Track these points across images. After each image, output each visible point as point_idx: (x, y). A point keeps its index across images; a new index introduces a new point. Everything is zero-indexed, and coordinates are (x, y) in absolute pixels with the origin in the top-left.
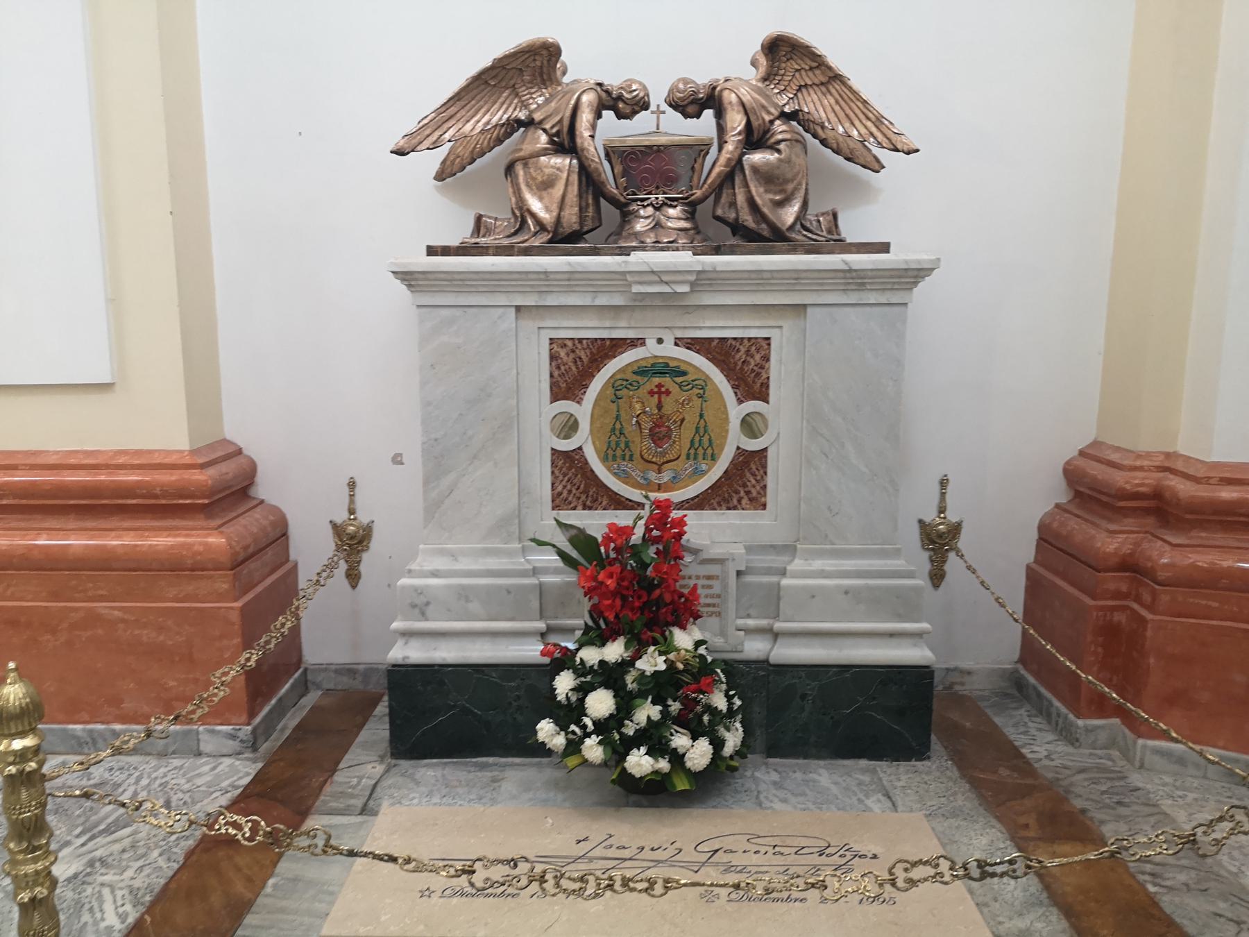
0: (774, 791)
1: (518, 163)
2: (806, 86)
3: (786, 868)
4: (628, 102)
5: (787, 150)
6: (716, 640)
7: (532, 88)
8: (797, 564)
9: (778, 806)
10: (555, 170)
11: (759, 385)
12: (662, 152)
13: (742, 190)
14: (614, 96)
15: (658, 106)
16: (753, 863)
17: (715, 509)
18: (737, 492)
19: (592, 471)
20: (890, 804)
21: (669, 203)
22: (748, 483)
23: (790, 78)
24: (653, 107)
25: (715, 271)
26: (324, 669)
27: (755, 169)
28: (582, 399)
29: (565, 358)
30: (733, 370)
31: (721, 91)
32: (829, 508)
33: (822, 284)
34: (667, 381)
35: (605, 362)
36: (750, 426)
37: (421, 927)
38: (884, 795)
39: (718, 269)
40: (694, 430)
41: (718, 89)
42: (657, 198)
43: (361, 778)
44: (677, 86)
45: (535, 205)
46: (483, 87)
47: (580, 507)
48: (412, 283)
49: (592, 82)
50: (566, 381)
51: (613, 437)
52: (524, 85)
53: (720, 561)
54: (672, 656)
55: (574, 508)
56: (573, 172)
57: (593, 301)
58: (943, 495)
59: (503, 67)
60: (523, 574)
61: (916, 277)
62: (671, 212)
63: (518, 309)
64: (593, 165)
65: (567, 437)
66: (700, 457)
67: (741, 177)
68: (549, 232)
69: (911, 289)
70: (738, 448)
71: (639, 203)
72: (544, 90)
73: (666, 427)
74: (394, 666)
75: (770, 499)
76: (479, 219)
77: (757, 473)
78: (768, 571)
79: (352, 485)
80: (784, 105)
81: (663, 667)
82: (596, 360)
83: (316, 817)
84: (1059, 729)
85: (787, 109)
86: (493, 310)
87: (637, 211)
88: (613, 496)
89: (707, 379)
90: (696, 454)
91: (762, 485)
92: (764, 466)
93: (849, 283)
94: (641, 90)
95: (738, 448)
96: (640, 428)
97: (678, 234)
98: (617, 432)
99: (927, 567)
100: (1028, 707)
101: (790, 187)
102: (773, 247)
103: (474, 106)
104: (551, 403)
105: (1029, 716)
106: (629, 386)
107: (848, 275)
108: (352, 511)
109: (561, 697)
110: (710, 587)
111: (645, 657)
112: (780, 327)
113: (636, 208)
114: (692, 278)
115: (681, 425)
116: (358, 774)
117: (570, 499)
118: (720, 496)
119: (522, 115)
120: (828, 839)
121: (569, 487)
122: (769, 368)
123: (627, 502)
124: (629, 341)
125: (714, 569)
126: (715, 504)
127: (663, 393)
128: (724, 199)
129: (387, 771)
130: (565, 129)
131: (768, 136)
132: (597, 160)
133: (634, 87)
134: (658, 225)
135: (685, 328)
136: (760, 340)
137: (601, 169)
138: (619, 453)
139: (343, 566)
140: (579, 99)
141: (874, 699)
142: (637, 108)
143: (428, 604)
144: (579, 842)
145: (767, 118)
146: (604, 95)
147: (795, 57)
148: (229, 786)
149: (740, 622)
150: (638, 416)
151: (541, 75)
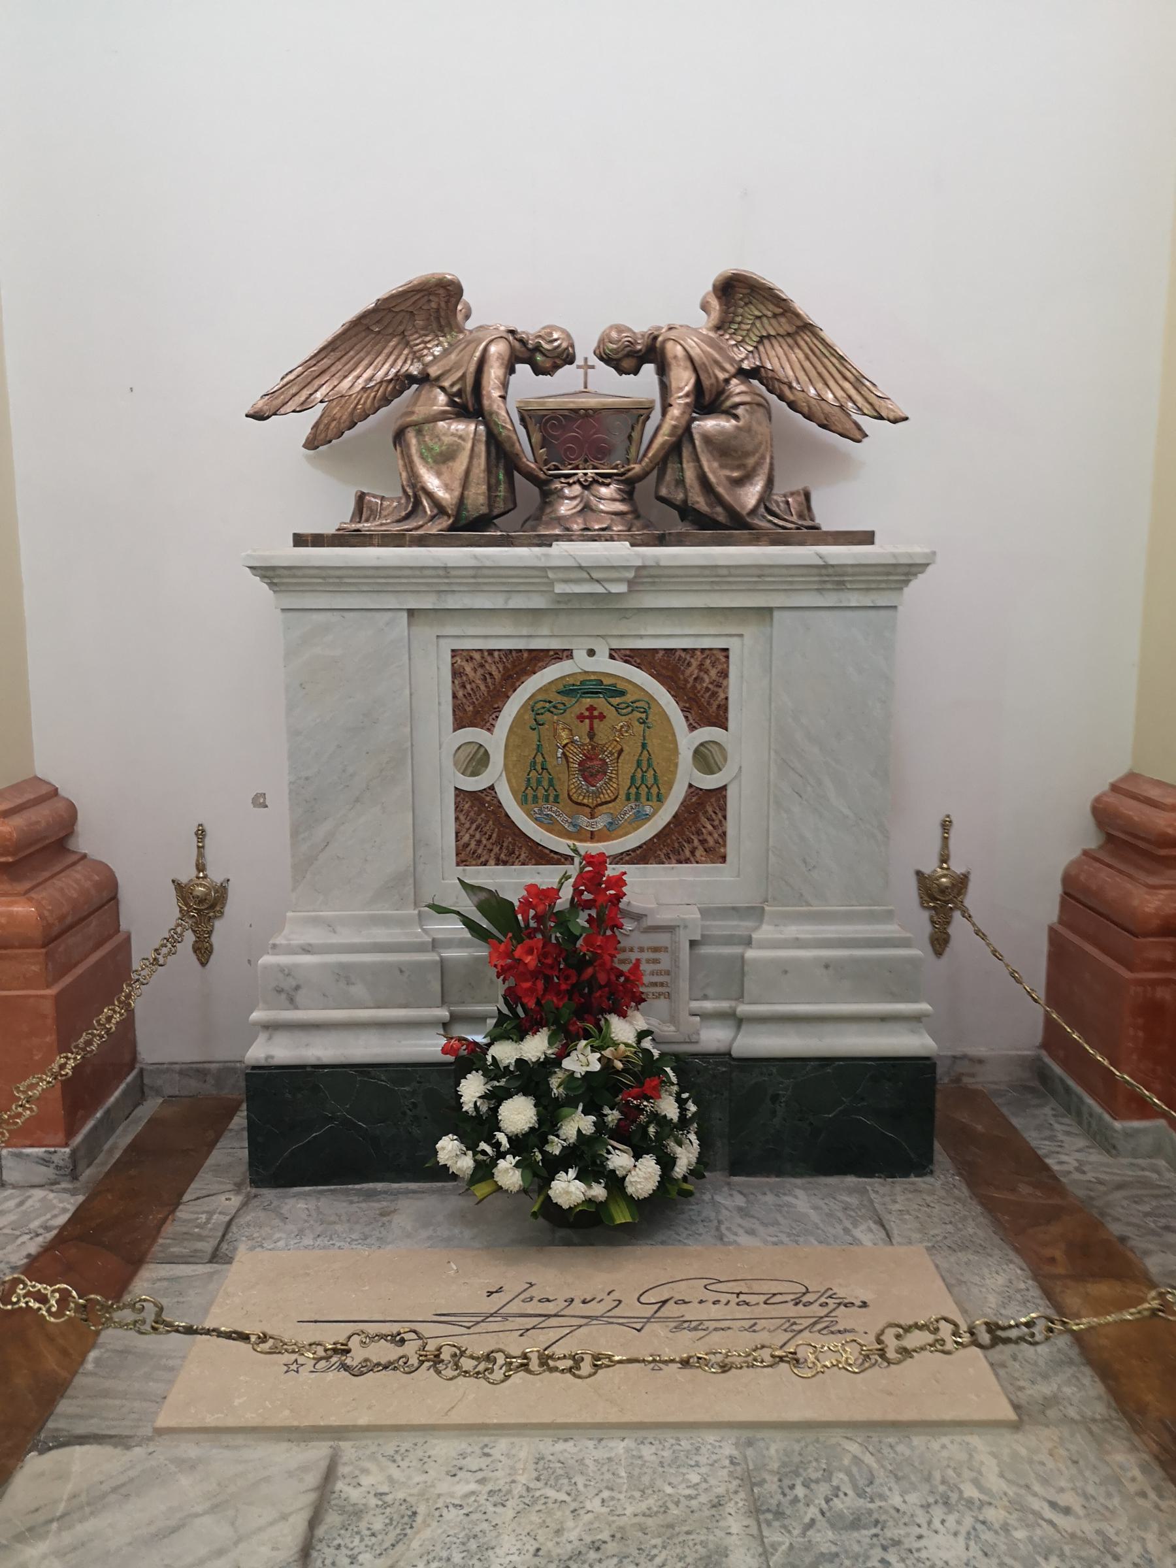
0: (740, 1221)
1: (409, 429)
2: (769, 337)
3: (753, 1322)
4: (546, 352)
5: (747, 416)
6: (666, 1029)
7: (426, 335)
8: (766, 932)
9: (744, 1239)
10: (456, 439)
11: (715, 707)
12: (591, 416)
13: (691, 464)
14: (530, 346)
15: (586, 359)
17: (663, 863)
18: (689, 841)
19: (507, 815)
20: (883, 1234)
21: (601, 480)
23: (749, 327)
24: (579, 361)
25: (659, 567)
27: (707, 439)
28: (493, 725)
29: (471, 674)
31: (664, 341)
32: (805, 861)
33: (791, 583)
34: (600, 702)
35: (523, 679)
36: (705, 758)
37: (287, 1413)
38: (875, 1222)
39: (662, 563)
41: (660, 339)
42: (585, 474)
43: (210, 1214)
44: (608, 335)
45: (432, 482)
46: (364, 334)
47: (492, 862)
48: (275, 581)
49: (502, 328)
51: (533, 773)
52: (416, 332)
53: (670, 929)
54: (608, 1053)
56: (479, 441)
57: (506, 602)
58: (945, 840)
59: (390, 310)
60: (420, 948)
61: (907, 574)
62: (604, 491)
63: (411, 612)
64: (504, 433)
65: (474, 774)
67: (690, 449)
68: (449, 516)
69: (901, 589)
70: (690, 786)
71: (563, 480)
72: (441, 339)
73: (600, 759)
74: (254, 1068)
75: (730, 850)
76: (361, 497)
77: (714, 816)
78: (729, 940)
79: (201, 834)
80: (742, 360)
81: (596, 1067)
82: (511, 677)
83: (152, 1266)
85: (746, 365)
86: (377, 615)
87: (562, 489)
88: (535, 847)
89: (651, 700)
91: (720, 831)
92: (723, 809)
93: (825, 582)
94: (563, 339)
95: (690, 786)
96: (568, 762)
97: (612, 520)
98: (539, 767)
101: (751, 461)
102: (731, 536)
103: (353, 358)
104: (455, 730)
105: (1054, 1116)
107: (824, 571)
108: (201, 867)
109: (468, 1107)
110: (656, 961)
111: (574, 1054)
112: (741, 636)
113: (559, 486)
114: (630, 575)
115: (618, 758)
116: (206, 1209)
117: (479, 851)
118: (668, 845)
119: (415, 369)
122: (727, 687)
123: (552, 855)
125: (662, 939)
126: (663, 856)
127: (596, 717)
128: (669, 476)
129: (245, 1204)
130: (469, 389)
131: (722, 398)
132: (509, 427)
133: (555, 336)
134: (587, 509)
136: (715, 652)
137: (515, 437)
139: (190, 937)
140: (485, 350)
141: (863, 1099)
142: (559, 362)
143: (297, 988)
144: (490, 1293)
145: (722, 376)
146: (517, 344)
147: (754, 301)
148: (41, 1227)
149: (695, 1005)
150: (564, 746)
151: (438, 319)
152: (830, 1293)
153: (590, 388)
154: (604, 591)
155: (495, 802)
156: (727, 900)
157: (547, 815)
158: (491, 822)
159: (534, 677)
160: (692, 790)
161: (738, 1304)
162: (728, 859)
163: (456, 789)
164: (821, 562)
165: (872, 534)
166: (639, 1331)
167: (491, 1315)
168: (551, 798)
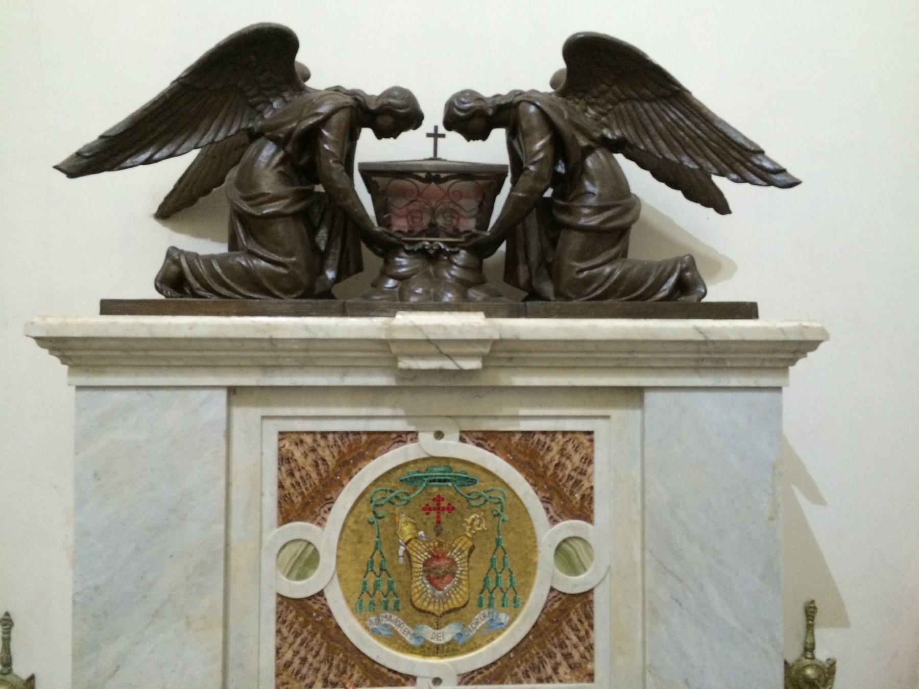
17: (520, 682)
18: (551, 655)
19: (338, 627)
22: (567, 642)
48: (68, 353)
50: (302, 493)
51: (370, 574)
61: (795, 352)
63: (232, 391)
65: (301, 576)
66: (497, 603)
70: (552, 589)
73: (449, 558)
75: (600, 664)
77: (579, 626)
82: (346, 463)
86: (192, 394)
88: (369, 665)
90: (491, 598)
91: (586, 644)
92: (589, 616)
93: (703, 359)
98: (377, 570)
106: (394, 500)
114: (486, 350)
117: (304, 671)
118: (526, 661)
121: (302, 653)
122: (591, 475)
123: (391, 674)
124: (394, 436)
127: (444, 509)
150: (407, 543)
157: (386, 625)
158: (319, 636)
159: (373, 463)
160: (554, 594)
162: (598, 677)
164: (700, 338)
168: (391, 605)
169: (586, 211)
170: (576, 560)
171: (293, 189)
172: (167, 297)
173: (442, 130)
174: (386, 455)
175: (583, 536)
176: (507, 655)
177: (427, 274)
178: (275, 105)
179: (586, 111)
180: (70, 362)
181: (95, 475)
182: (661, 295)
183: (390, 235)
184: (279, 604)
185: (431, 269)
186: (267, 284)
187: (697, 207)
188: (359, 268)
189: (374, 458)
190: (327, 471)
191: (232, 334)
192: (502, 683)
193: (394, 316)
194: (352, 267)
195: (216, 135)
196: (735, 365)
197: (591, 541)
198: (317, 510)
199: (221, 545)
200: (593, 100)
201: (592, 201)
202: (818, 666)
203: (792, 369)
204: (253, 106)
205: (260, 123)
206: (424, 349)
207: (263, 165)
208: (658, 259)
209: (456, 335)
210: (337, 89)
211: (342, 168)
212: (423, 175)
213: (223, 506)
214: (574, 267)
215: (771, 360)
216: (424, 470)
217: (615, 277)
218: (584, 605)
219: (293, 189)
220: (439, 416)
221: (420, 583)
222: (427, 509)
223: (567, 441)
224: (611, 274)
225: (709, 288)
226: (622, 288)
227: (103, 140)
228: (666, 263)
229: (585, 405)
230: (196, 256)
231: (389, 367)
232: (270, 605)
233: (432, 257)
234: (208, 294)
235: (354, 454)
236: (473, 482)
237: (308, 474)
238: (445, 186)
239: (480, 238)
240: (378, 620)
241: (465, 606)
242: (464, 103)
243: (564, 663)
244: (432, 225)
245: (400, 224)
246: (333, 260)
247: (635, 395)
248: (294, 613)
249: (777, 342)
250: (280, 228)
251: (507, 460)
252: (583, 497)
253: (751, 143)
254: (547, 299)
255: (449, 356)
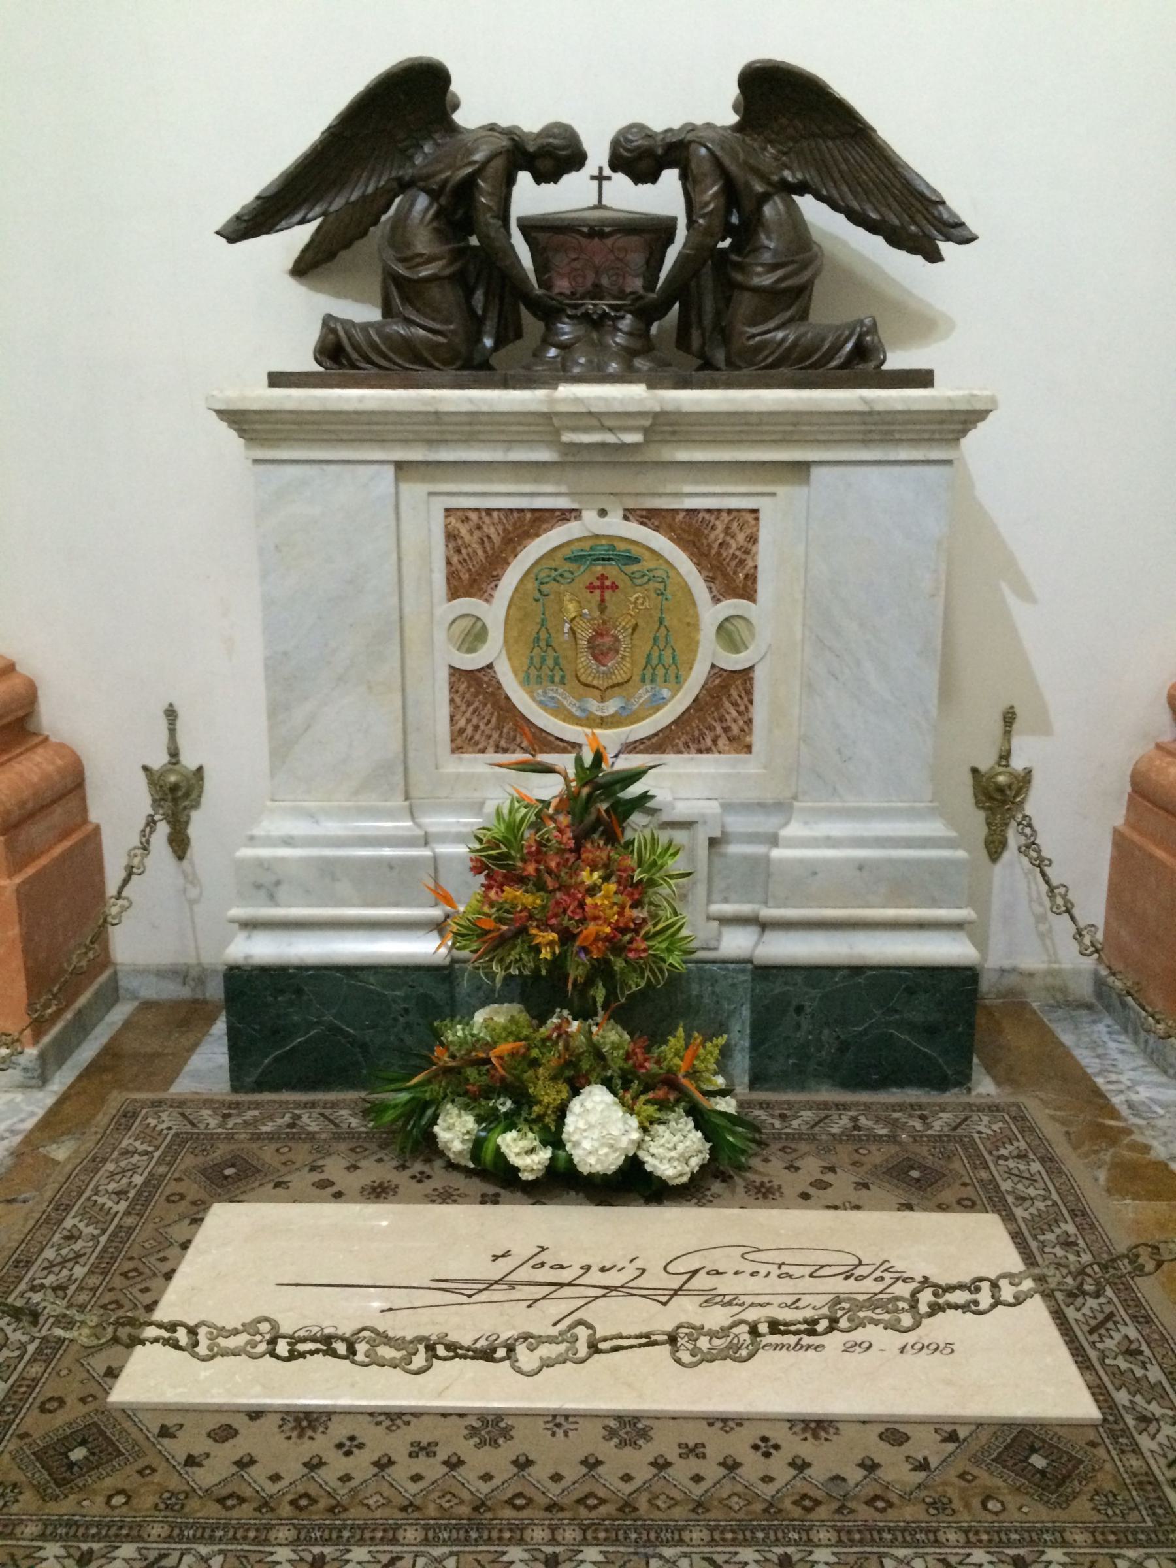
3: (796, 1297)
8: (794, 829)
16: (749, 1290)
17: (681, 752)
18: (711, 728)
19: (507, 698)
22: (727, 716)
26: (140, 972)
30: (707, 556)
32: (839, 751)
34: (612, 571)
36: (729, 635)
40: (651, 642)
47: (491, 749)
48: (245, 427)
50: (469, 570)
51: (537, 650)
53: (686, 825)
55: (483, 751)
58: (172, 731)
60: (409, 842)
61: (965, 422)
63: (399, 466)
65: (471, 650)
66: (659, 680)
69: (958, 439)
70: (713, 666)
73: (613, 636)
75: (758, 738)
77: (739, 701)
79: (171, 714)
82: (511, 540)
84: (1149, 1050)
86: (361, 469)
88: (538, 733)
90: (653, 675)
91: (746, 719)
92: (749, 692)
93: (870, 431)
98: (543, 644)
99: (982, 831)
100: (1108, 1021)
105: (1110, 1033)
106: (559, 578)
108: (174, 754)
114: (647, 423)
117: (477, 737)
118: (687, 733)
120: (859, 1254)
121: (475, 721)
122: (756, 553)
123: (558, 743)
124: (558, 513)
125: (680, 837)
127: (607, 587)
135: (637, 494)
138: (546, 671)
139: (163, 829)
143: (278, 883)
148: (7, 1130)
150: (572, 620)
152: (886, 1266)
153: (604, 203)
154: (617, 441)
155: (494, 683)
156: (750, 794)
157: (553, 698)
158: (489, 706)
159: (538, 541)
160: (716, 671)
161: (779, 1276)
162: (754, 749)
163: (451, 667)
164: (865, 408)
165: (930, 373)
166: (664, 1304)
167: (496, 1282)
168: (557, 679)
169: (759, 269)
170: (738, 638)
171: (446, 248)
172: (326, 368)
173: (607, 172)
174: (550, 533)
175: (746, 615)
176: (669, 726)
177: (592, 344)
178: (427, 149)
179: (765, 149)
180: (247, 436)
181: (277, 547)
182: (834, 363)
183: (553, 299)
184: (451, 675)
185: (595, 336)
186: (426, 354)
187: (903, 254)
188: (519, 335)
189: (538, 535)
190: (493, 549)
191: (399, 407)
192: (663, 752)
193: (556, 388)
194: (511, 335)
195: (367, 186)
196: (904, 437)
197: (754, 621)
198: (484, 586)
199: (395, 616)
200: (773, 136)
201: (767, 257)
202: (1011, 774)
203: (963, 441)
204: (403, 151)
205: (410, 171)
206: (586, 421)
207: (417, 221)
208: (837, 322)
209: (618, 408)
210: (492, 128)
211: (500, 223)
212: (586, 230)
213: (396, 579)
214: (746, 332)
215: (940, 432)
216: (588, 548)
217: (787, 344)
218: (745, 682)
219: (446, 248)
220: (603, 494)
221: (585, 660)
222: (591, 588)
223: (732, 520)
224: (784, 340)
225: (888, 355)
226: (795, 356)
227: (259, 202)
228: (847, 325)
229: (750, 481)
230: (353, 324)
231: (551, 442)
232: (443, 677)
233: (597, 322)
234: (367, 366)
235: (520, 531)
236: (636, 560)
237: (475, 552)
238: (609, 242)
239: (647, 300)
240: (545, 693)
241: (628, 681)
242: (632, 141)
243: (724, 737)
244: (597, 286)
245: (562, 285)
246: (490, 326)
247: (801, 470)
248: (465, 684)
249: (941, 412)
250: (435, 293)
251: (671, 539)
252: (747, 576)
253: (934, 191)
254: (718, 369)
255: (611, 430)
